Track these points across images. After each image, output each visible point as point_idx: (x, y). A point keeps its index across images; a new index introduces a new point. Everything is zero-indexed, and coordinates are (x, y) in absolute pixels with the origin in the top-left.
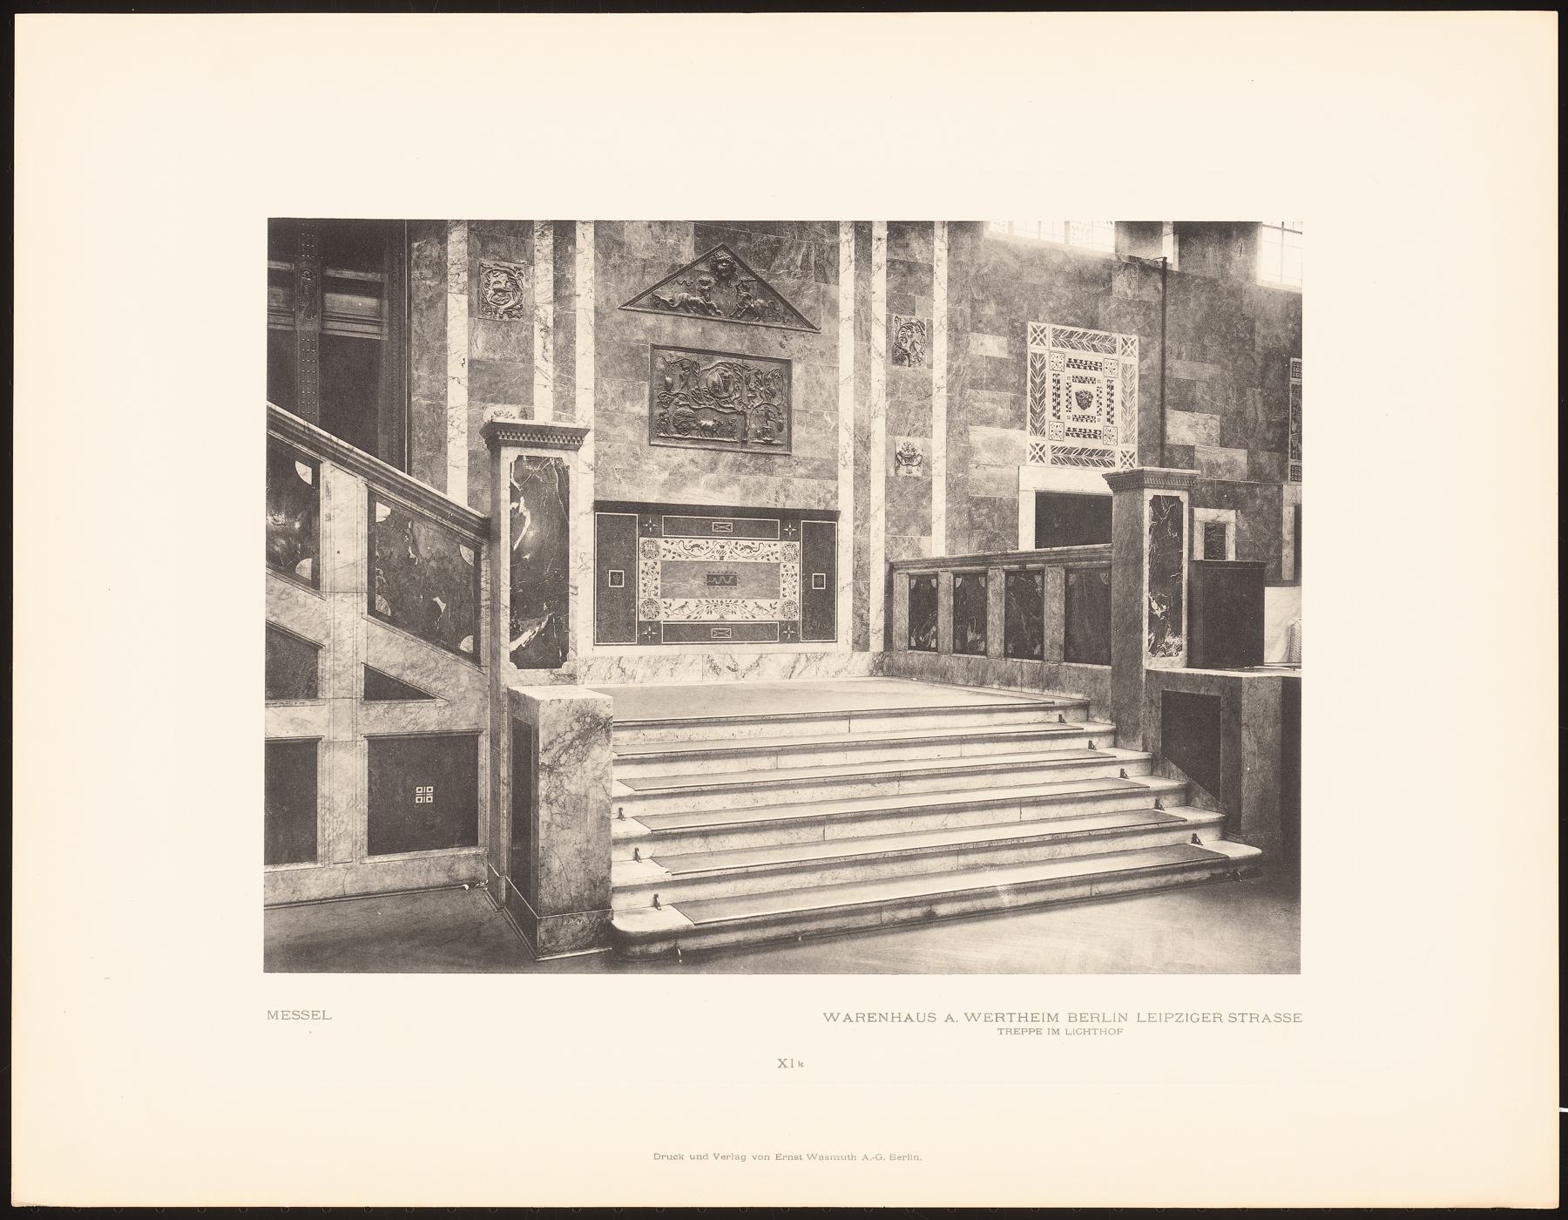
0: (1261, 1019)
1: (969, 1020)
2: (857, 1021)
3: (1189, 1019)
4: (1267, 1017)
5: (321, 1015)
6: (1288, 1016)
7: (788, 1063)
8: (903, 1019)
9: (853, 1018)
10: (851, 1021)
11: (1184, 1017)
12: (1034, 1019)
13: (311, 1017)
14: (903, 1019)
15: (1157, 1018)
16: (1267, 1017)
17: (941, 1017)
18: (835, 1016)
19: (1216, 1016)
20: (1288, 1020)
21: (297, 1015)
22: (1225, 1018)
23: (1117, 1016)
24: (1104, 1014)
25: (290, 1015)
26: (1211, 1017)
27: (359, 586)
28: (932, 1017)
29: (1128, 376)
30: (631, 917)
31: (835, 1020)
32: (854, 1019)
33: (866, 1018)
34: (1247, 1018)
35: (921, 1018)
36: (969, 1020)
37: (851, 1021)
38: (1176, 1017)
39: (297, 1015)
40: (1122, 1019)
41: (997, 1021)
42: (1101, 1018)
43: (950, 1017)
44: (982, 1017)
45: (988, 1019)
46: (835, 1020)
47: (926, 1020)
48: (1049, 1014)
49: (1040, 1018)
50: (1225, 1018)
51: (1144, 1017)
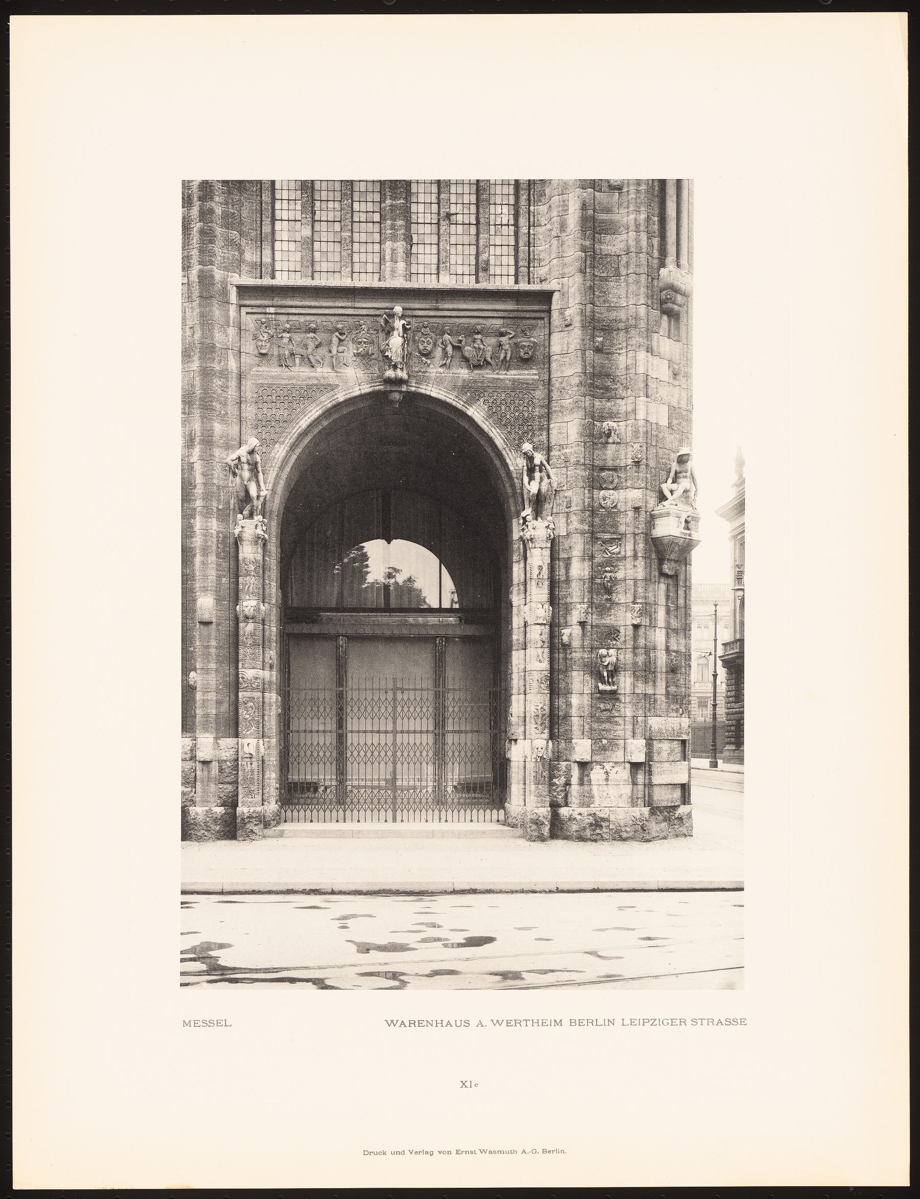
0: (715, 1023)
1: (389, 1026)
2: (410, 1026)
3: (661, 1023)
4: (449, 1023)
5: (223, 1023)
6: (205, 1022)
7: (468, 1084)
8: (444, 1024)
9: (407, 1024)
10: (405, 1026)
11: (657, 1022)
12: (742, 1023)
13: (216, 1025)
14: (444, 1024)
15: (637, 1022)
16: (449, 1023)
17: (473, 1023)
18: (395, 1022)
19: (682, 1020)
20: (213, 1025)
21: (208, 1023)
22: (689, 1022)
23: (607, 1021)
24: (597, 1020)
25: (200, 1023)
26: (513, 1023)
27: (620, 371)
28: (467, 1023)
29: (560, 781)
30: (625, 835)
31: (395, 1026)
32: (407, 1024)
33: (417, 1024)
34: (705, 1022)
35: (458, 1024)
36: (389, 1026)
37: (405, 1026)
38: (651, 1022)
39: (208, 1023)
40: (431, 1022)
41: (516, 1026)
42: (594, 1023)
43: (480, 1024)
44: (505, 1023)
45: (581, 1024)
46: (395, 1026)
47: (463, 1025)
48: (555, 1021)
49: (637, 1022)
50: (689, 1022)
51: (627, 1022)
